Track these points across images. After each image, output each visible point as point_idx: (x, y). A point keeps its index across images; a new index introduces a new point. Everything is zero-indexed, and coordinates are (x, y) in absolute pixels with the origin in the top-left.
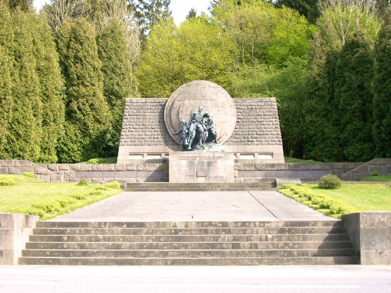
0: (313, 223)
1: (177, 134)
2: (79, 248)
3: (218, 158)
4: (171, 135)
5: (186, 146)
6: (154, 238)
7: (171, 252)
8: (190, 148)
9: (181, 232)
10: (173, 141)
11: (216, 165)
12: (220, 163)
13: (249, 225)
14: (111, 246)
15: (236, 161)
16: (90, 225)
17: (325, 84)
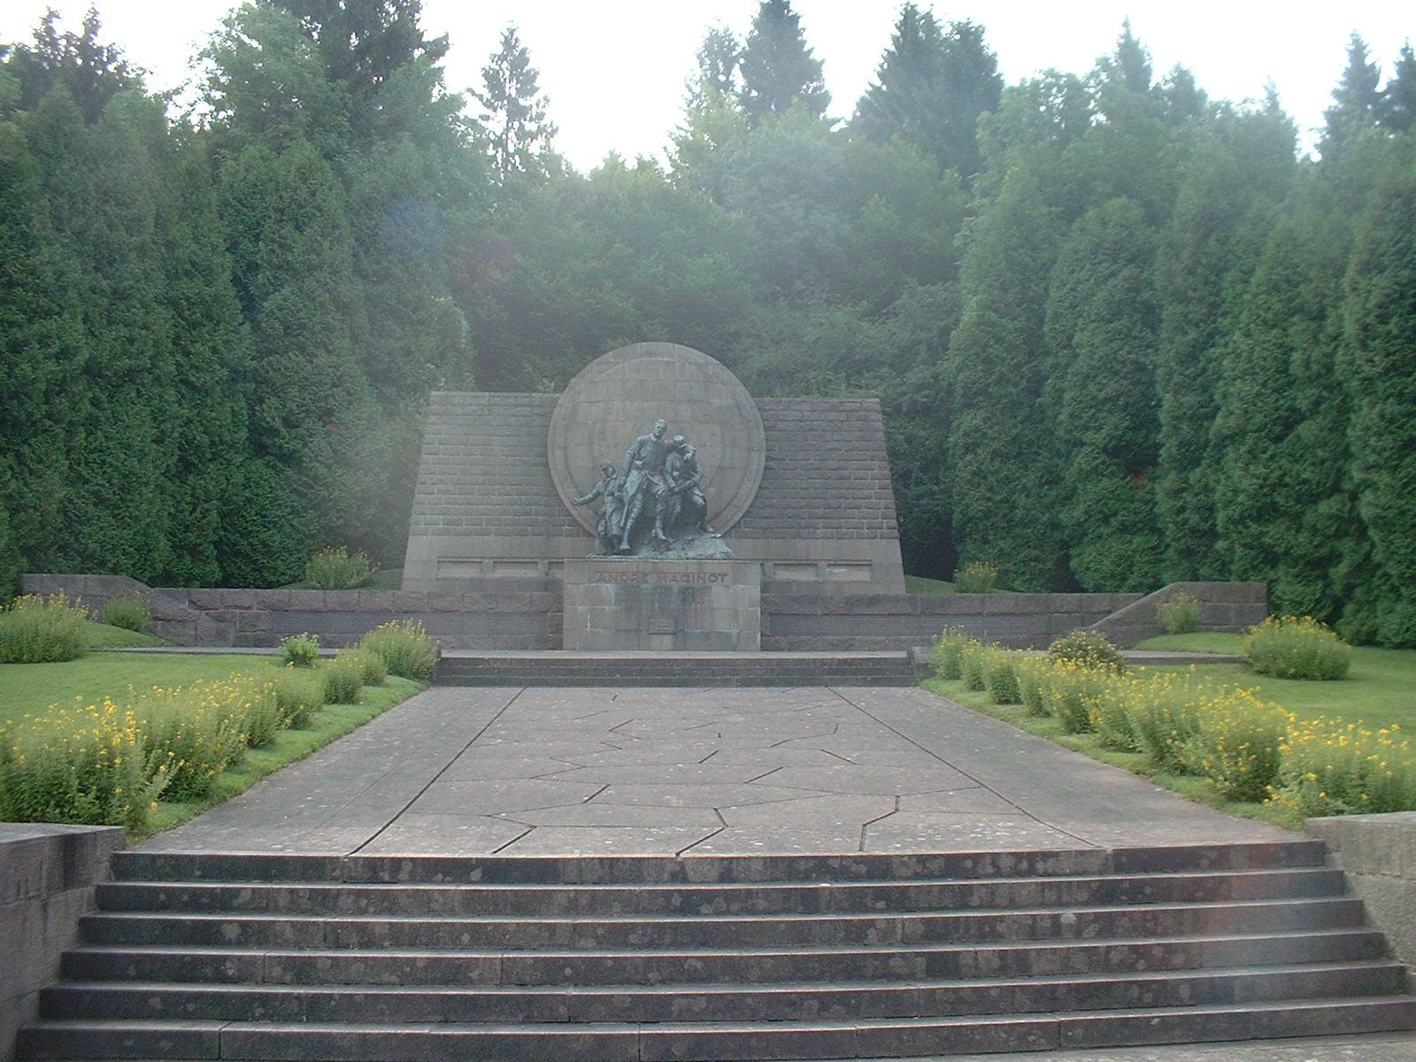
0: (1214, 855)
1: (586, 503)
2: (288, 978)
3: (713, 579)
4: (568, 505)
5: (615, 541)
6: (600, 931)
7: (682, 1001)
8: (625, 546)
9: (710, 902)
10: (574, 523)
11: (706, 598)
12: (719, 595)
13: (974, 867)
14: (425, 968)
15: (765, 587)
16: (334, 870)
17: (1018, 366)
